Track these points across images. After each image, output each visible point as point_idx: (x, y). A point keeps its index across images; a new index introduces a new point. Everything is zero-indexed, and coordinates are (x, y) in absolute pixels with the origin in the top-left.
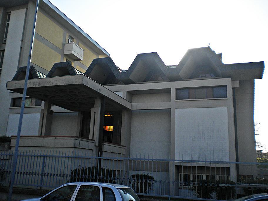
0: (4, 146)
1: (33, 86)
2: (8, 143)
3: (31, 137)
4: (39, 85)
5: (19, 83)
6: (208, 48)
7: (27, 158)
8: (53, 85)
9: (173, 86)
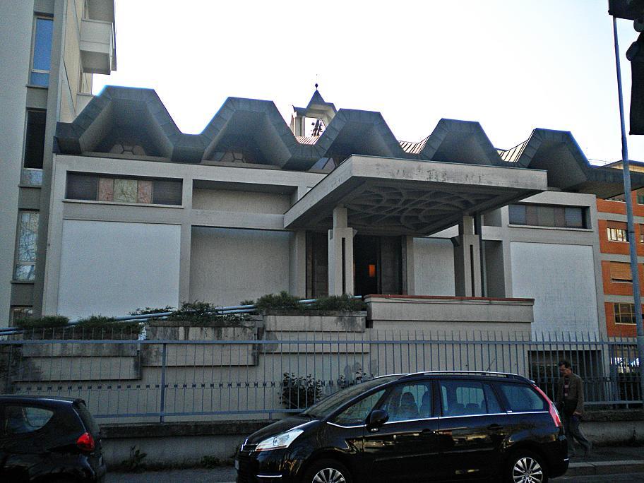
0: (352, 321)
1: (430, 178)
2: (363, 314)
3: (429, 300)
4: (445, 177)
5: (387, 166)
6: (537, 132)
7: (390, 348)
8: (481, 184)
9: (189, 173)
